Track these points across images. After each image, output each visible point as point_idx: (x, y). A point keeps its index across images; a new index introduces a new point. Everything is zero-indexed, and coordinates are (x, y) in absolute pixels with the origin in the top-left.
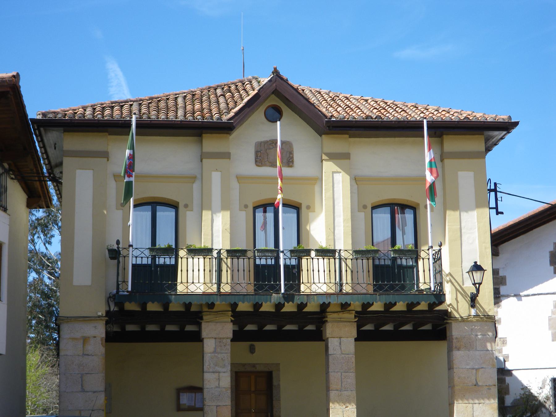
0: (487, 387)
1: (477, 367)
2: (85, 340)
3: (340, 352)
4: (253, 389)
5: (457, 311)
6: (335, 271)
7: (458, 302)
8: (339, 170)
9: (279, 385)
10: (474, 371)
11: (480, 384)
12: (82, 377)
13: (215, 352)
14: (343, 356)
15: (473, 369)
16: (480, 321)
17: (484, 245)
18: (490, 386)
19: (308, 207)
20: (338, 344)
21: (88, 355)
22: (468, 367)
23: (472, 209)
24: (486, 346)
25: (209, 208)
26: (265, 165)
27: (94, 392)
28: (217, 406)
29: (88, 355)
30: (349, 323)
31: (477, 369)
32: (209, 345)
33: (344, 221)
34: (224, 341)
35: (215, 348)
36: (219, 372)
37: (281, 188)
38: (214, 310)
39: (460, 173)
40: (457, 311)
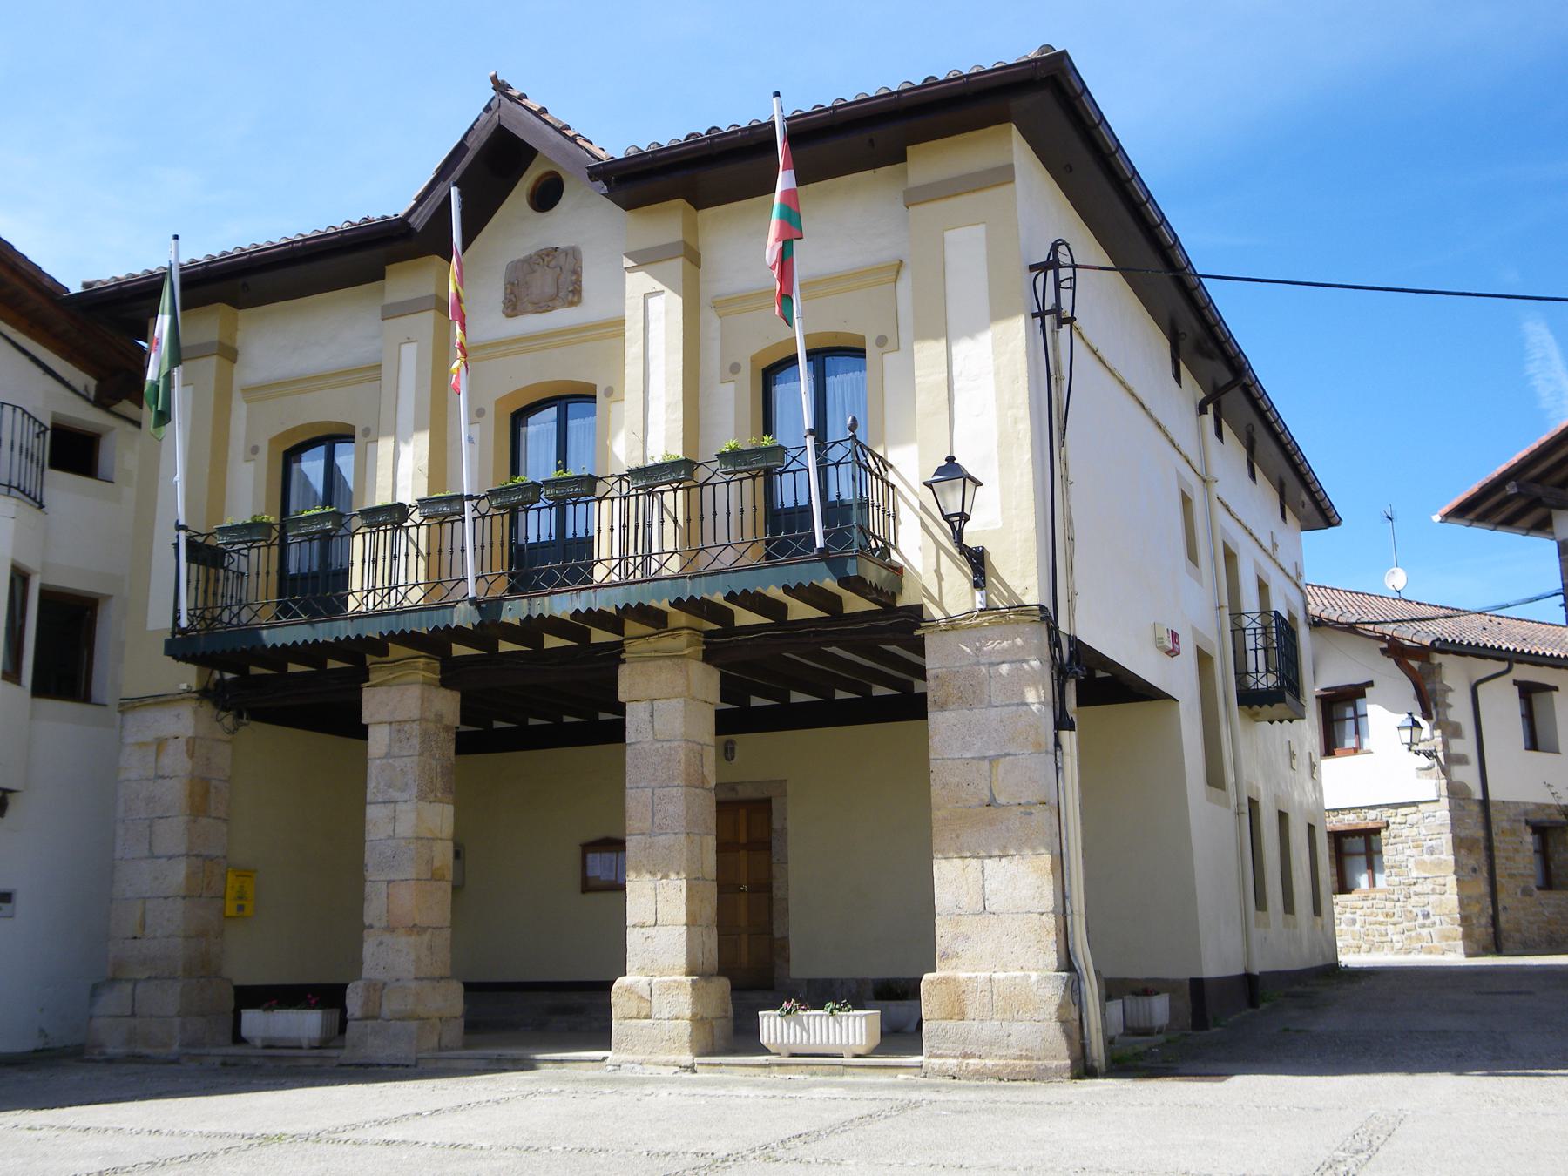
0: (1021, 809)
1: (991, 753)
2: (160, 743)
3: (650, 737)
4: (743, 839)
5: (939, 605)
6: (612, 529)
7: (940, 578)
8: (659, 286)
9: (784, 829)
10: (986, 763)
11: (1002, 799)
12: (150, 826)
13: (388, 755)
14: (658, 745)
15: (983, 758)
16: (998, 623)
17: (1010, 413)
18: (1029, 804)
19: (609, 392)
20: (647, 716)
21: (163, 777)
22: (968, 755)
23: (985, 328)
24: (1022, 694)
25: (394, 432)
26: (526, 312)
27: (170, 858)
28: (389, 882)
29: (163, 777)
30: (669, 662)
31: (992, 760)
32: (378, 739)
33: (668, 406)
34: (407, 727)
35: (390, 746)
36: (395, 802)
37: (461, 346)
38: (390, 658)
39: (950, 235)
40: (939, 605)
